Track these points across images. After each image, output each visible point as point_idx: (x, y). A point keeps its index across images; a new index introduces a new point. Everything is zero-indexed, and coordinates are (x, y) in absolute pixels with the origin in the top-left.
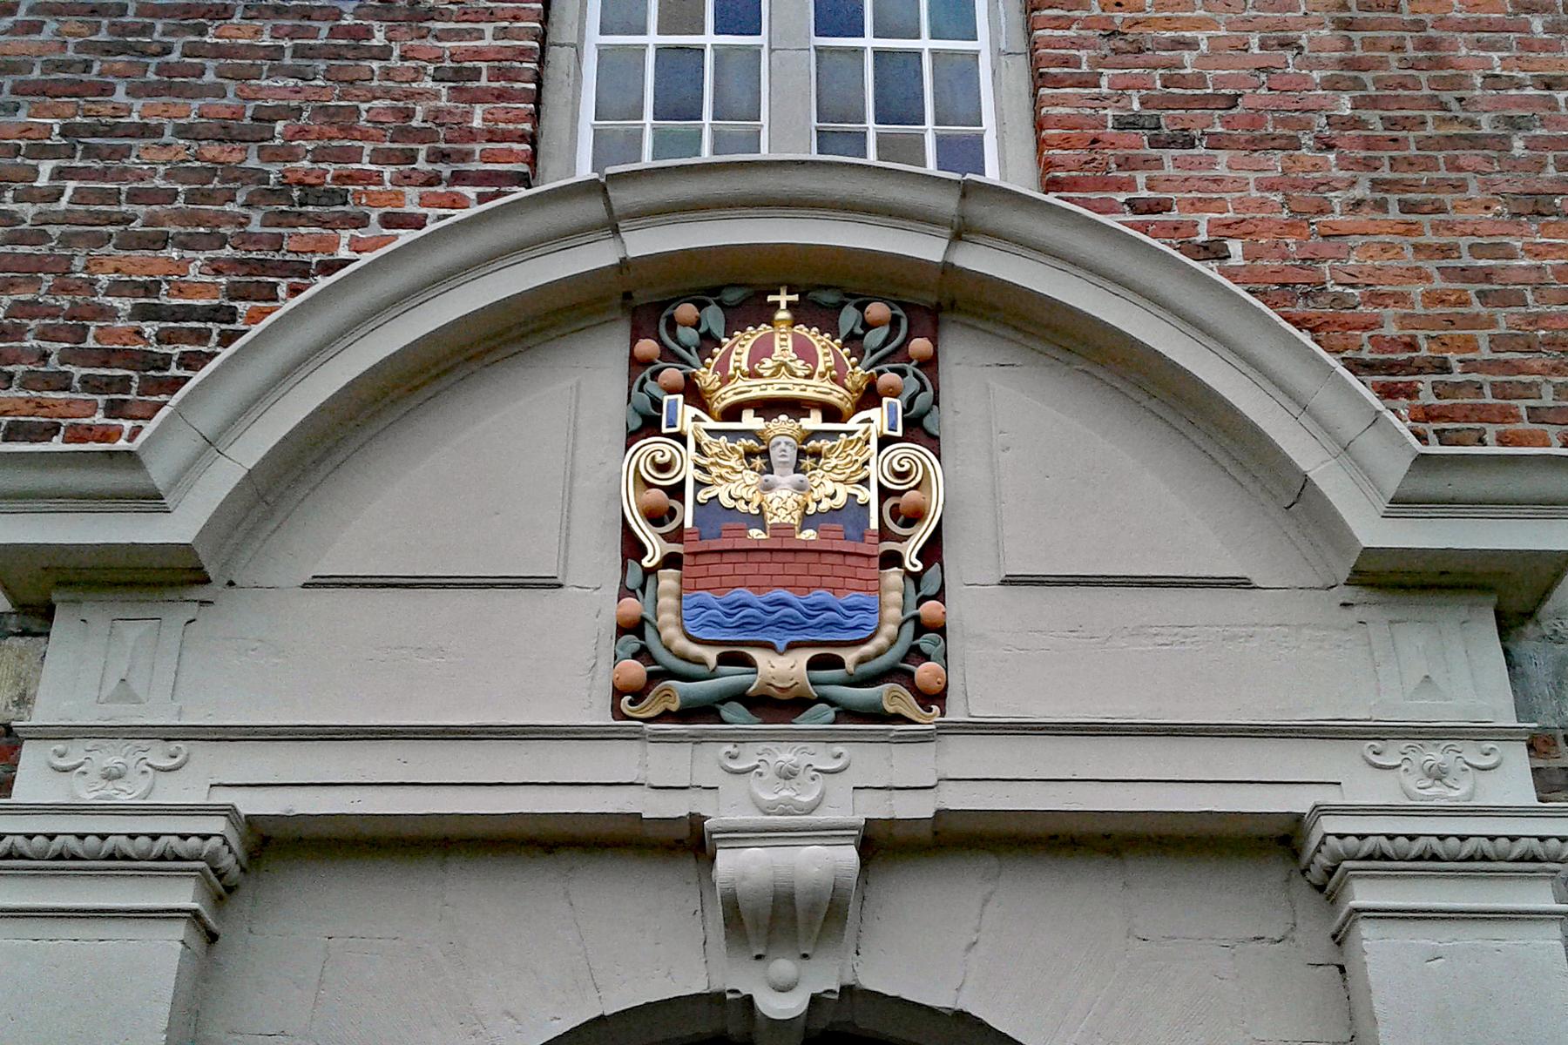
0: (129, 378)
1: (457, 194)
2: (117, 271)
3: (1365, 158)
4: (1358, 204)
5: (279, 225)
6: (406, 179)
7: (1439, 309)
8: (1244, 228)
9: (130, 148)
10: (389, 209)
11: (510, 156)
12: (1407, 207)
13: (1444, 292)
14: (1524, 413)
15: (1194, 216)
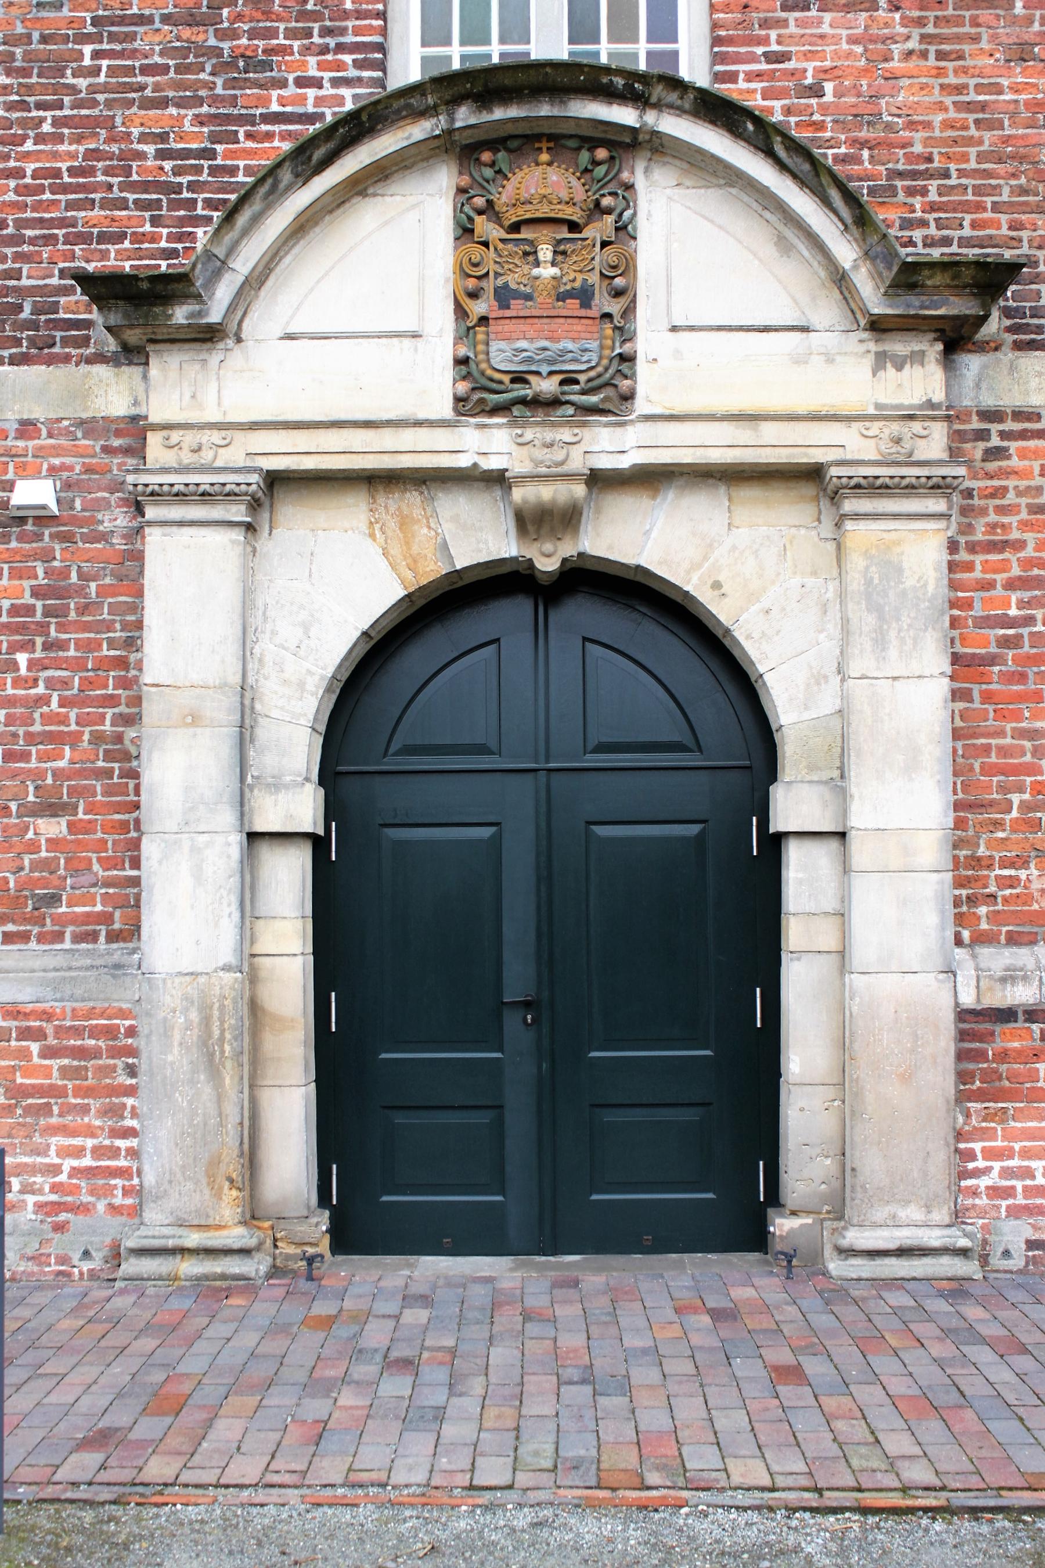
0: (161, 200)
1: (340, 60)
2: (142, 125)
3: (919, 17)
4: (910, 53)
5: (234, 88)
6: (306, 50)
7: (950, 133)
8: (837, 73)
9: (135, 33)
10: (299, 73)
11: (370, 30)
12: (941, 56)
13: (955, 120)
14: (989, 206)
15: (805, 65)
